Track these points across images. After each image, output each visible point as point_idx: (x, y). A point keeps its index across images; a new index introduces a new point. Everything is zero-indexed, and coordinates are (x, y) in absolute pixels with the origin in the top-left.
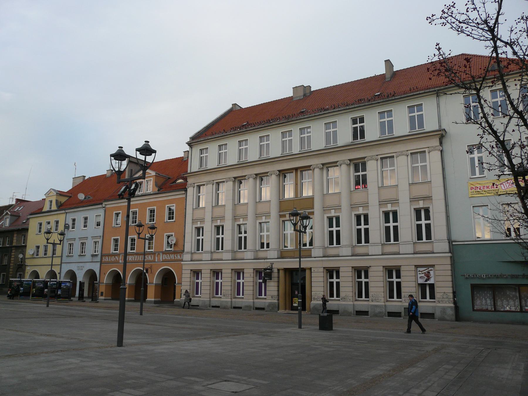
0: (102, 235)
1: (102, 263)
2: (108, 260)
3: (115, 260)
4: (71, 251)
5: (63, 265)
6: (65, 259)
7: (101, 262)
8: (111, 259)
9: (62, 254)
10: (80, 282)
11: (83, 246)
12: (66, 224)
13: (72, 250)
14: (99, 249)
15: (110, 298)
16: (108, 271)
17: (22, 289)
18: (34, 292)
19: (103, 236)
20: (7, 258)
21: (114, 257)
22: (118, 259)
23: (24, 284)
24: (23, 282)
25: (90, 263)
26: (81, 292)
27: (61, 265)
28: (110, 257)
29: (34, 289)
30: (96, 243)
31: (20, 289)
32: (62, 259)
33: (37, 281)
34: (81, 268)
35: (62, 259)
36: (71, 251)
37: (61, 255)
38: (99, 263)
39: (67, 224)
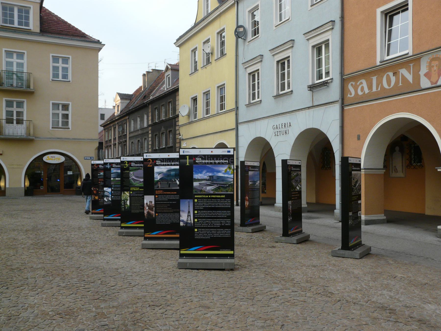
0: (336, 16)
1: (346, 103)
2: (366, 91)
3: (397, 82)
4: (256, 82)
5: (241, 127)
6: (244, 113)
7: (343, 103)
8: (379, 82)
9: (237, 102)
10: (284, 162)
11: (284, 69)
12: (238, 27)
13: (258, 88)
14: (331, 65)
15: (382, 217)
16: (372, 127)
17: (109, 190)
18: (128, 203)
19: (342, 18)
20: (172, 136)
21: (391, 74)
22: (410, 77)
23: (112, 175)
24: (110, 170)
25: (307, 111)
26: (290, 202)
27: (237, 129)
28: (374, 79)
29: (127, 194)
30: (318, 49)
31: (104, 191)
32: (237, 115)
33: (133, 164)
34: (284, 129)
35: (237, 115)
36: (256, 91)
37: (234, 106)
38: (336, 108)
39: (241, 26)
